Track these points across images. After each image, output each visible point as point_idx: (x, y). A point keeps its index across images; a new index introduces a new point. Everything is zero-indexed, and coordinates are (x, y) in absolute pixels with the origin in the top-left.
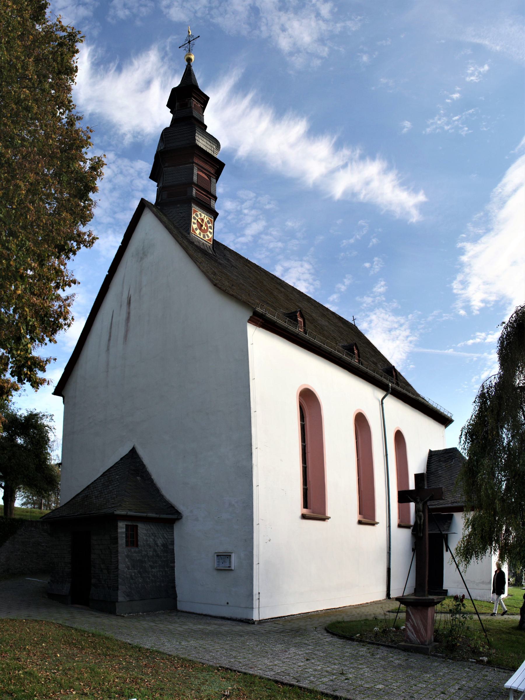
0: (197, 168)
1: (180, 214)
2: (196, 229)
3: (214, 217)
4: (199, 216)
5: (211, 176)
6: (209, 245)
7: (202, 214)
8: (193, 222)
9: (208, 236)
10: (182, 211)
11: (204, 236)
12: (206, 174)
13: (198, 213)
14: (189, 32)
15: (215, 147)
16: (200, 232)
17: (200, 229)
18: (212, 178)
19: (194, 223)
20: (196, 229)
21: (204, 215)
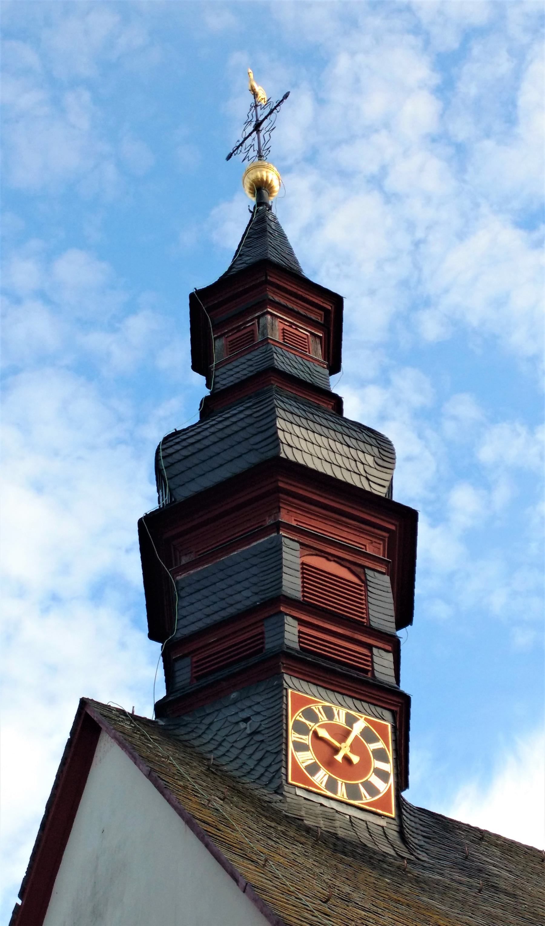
0: (297, 546)
1: (242, 725)
2: (313, 769)
3: (394, 713)
4: (323, 718)
5: (363, 567)
6: (383, 823)
7: (335, 709)
8: (386, 760)
9: (372, 789)
10: (244, 715)
11: (353, 792)
12: (340, 561)
13: (317, 708)
14: (255, 95)
15: (370, 460)
16: (331, 780)
17: (330, 764)
18: (367, 571)
19: (300, 747)
20: (313, 769)
21: (343, 712)
